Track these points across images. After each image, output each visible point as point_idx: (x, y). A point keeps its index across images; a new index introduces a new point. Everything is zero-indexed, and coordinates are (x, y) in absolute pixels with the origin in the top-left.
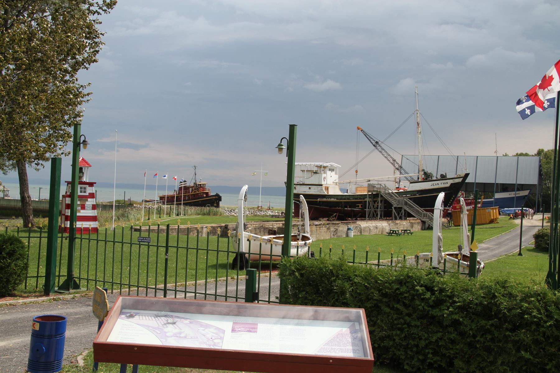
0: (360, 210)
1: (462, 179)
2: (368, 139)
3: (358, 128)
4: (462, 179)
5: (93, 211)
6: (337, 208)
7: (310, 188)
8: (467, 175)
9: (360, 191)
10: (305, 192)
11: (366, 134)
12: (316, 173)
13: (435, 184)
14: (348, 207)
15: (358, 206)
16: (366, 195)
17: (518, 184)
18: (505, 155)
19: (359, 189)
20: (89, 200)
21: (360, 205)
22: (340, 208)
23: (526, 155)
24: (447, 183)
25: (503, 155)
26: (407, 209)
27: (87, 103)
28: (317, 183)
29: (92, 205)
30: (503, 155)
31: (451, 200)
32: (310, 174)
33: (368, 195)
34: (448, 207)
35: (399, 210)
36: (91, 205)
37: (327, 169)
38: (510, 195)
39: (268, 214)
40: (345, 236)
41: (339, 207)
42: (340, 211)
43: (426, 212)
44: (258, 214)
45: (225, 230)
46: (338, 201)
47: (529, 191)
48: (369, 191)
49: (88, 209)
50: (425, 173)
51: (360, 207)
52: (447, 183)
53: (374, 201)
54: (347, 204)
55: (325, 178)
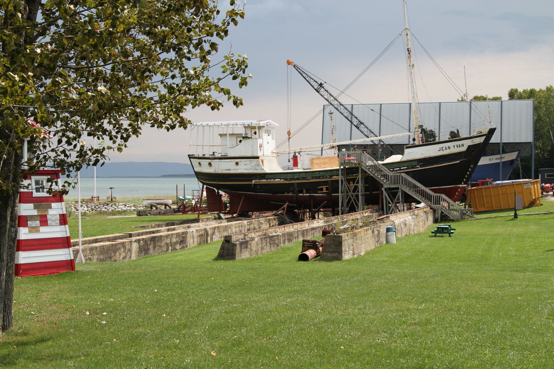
0: (324, 195)
1: (484, 137)
2: (304, 78)
3: (289, 63)
4: (484, 137)
5: (63, 227)
6: (286, 194)
7: (210, 164)
8: (492, 131)
9: (317, 164)
10: (229, 170)
11: (301, 73)
12: (246, 138)
13: (444, 149)
14: (304, 191)
15: (322, 189)
16: (338, 170)
17: (504, 143)
18: (460, 99)
19: (315, 161)
20: (54, 205)
22: (290, 194)
23: (484, 99)
24: (463, 145)
25: (458, 100)
26: (407, 191)
28: (249, 155)
29: (60, 215)
30: (458, 100)
31: (468, 173)
32: (234, 140)
33: (340, 171)
34: (464, 184)
35: (393, 193)
36: (58, 216)
37: (263, 130)
38: (490, 160)
39: (120, 210)
40: (385, 242)
41: (288, 193)
42: (290, 200)
43: (435, 193)
44: (103, 209)
45: (226, 245)
46: (287, 182)
47: (518, 152)
48: (341, 164)
49: (54, 224)
50: (423, 131)
51: (325, 191)
52: (463, 145)
53: (347, 180)
54: (302, 187)
55: (261, 146)
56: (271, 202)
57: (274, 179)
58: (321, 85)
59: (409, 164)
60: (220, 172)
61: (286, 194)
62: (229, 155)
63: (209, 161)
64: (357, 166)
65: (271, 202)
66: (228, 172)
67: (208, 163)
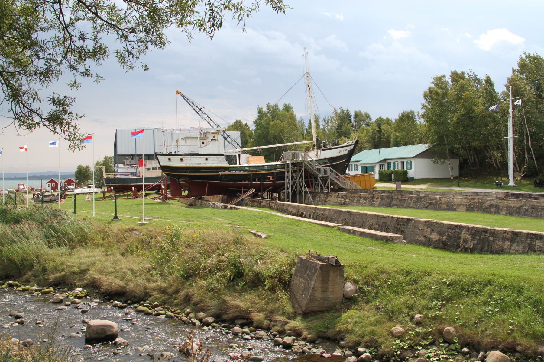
6: (243, 182)
7: (170, 159)
10: (200, 164)
11: (183, 96)
14: (257, 180)
15: (269, 178)
21: (271, 177)
22: (247, 182)
27: (126, 70)
41: (245, 181)
56: (228, 188)
57: (236, 171)
58: (201, 110)
59: (322, 161)
60: (191, 166)
61: (243, 182)
62: (200, 153)
63: (181, 157)
64: (302, 161)
65: (228, 188)
66: (199, 166)
67: (179, 159)
